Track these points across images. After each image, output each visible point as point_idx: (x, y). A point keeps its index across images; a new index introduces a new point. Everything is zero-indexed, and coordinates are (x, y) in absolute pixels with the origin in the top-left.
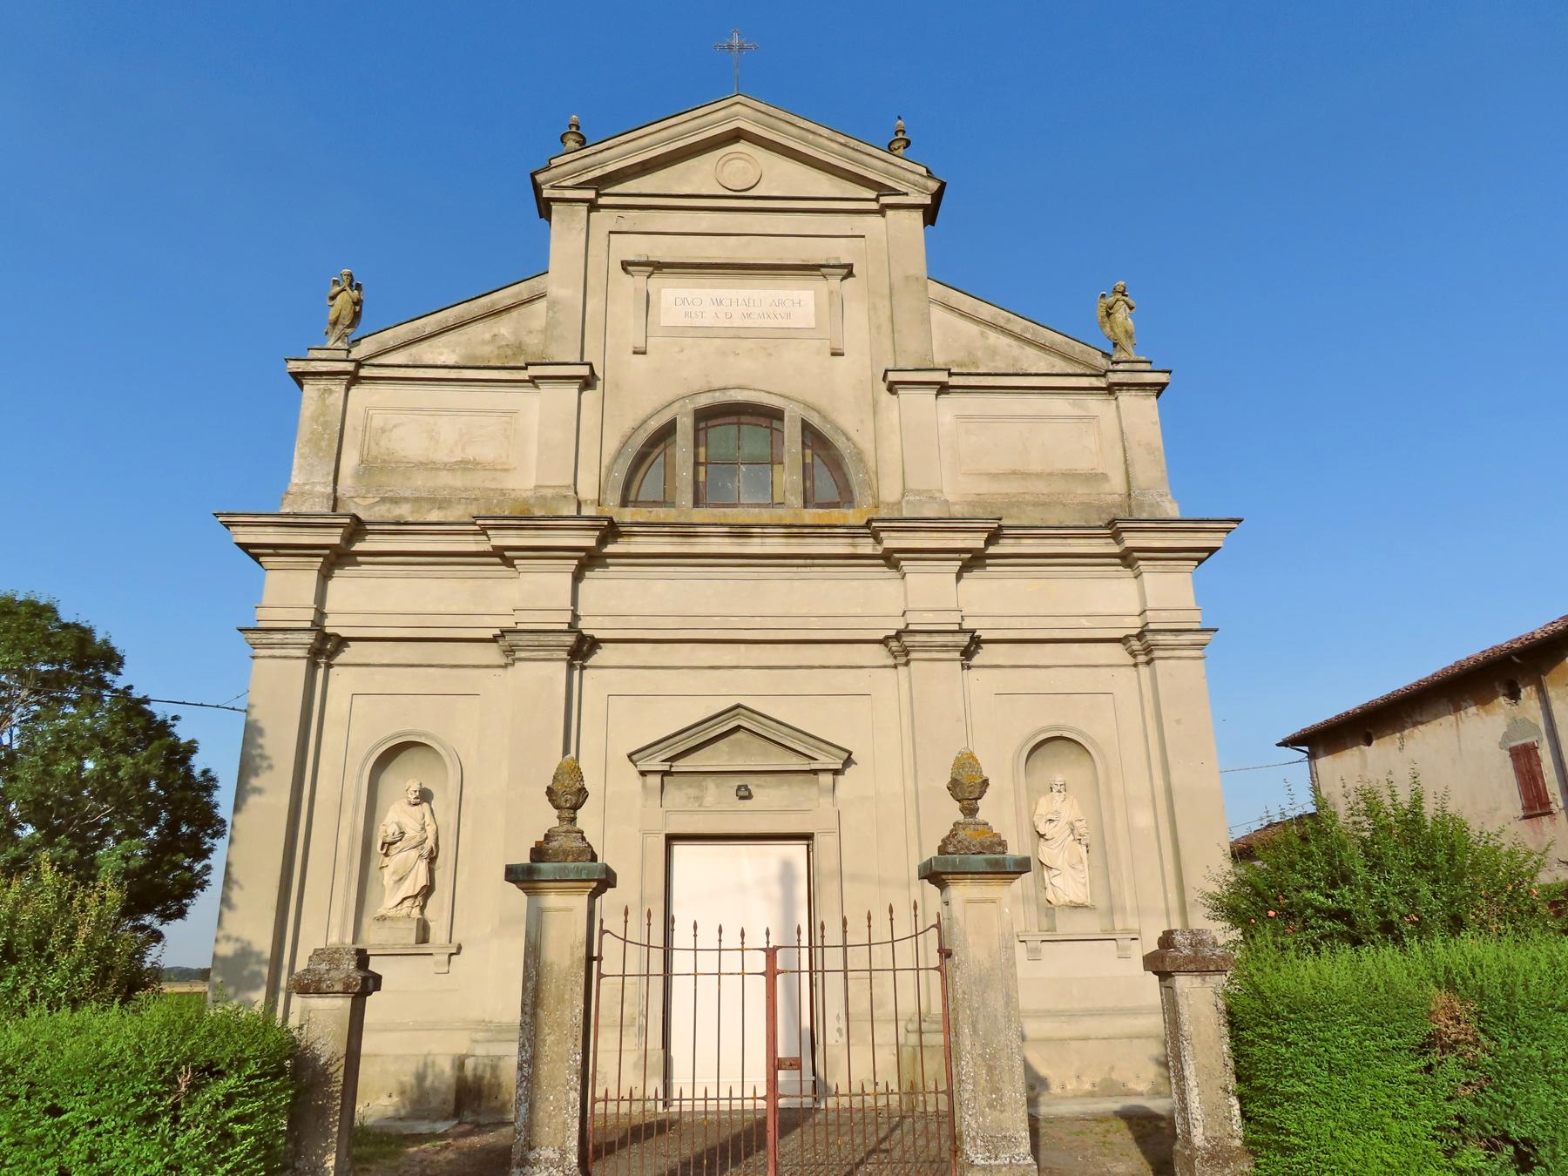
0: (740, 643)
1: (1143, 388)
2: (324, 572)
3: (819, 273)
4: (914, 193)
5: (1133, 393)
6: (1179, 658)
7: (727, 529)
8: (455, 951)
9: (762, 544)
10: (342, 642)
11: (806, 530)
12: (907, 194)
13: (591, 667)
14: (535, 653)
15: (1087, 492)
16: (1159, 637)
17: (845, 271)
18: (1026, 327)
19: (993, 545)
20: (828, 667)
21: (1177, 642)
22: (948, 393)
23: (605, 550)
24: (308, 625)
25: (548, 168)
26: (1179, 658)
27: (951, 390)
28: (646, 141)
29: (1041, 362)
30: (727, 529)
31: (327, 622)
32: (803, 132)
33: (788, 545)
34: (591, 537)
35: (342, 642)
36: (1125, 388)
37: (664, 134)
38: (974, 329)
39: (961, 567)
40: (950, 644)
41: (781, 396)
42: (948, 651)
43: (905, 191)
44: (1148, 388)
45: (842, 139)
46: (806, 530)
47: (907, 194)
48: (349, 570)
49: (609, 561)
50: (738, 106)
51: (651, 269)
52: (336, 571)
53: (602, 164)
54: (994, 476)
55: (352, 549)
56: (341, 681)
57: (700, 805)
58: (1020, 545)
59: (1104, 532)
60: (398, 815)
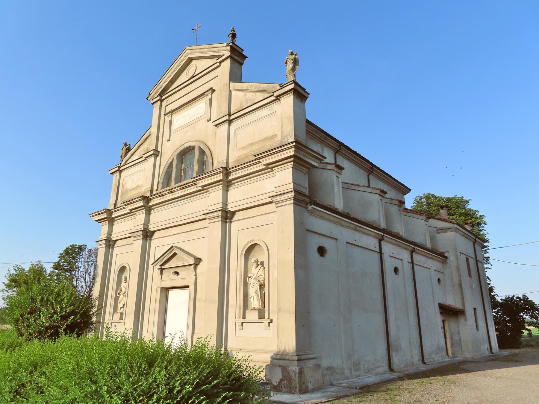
0: (185, 224)
1: (287, 93)
2: (226, 189)
3: (205, 95)
4: (226, 53)
5: (285, 97)
6: (284, 205)
7: (168, 191)
8: (270, 324)
9: (235, 174)
10: (234, 213)
11: (184, 186)
12: (224, 55)
13: (115, 247)
14: (138, 238)
15: (270, 144)
16: (276, 198)
17: (210, 91)
18: (251, 86)
19: (230, 176)
20: (203, 228)
21: (282, 199)
22: (233, 122)
23: (149, 205)
24: (292, 190)
25: (149, 95)
26: (284, 205)
27: (233, 121)
28: (168, 75)
29: (260, 96)
30: (168, 191)
31: (228, 207)
32: (200, 50)
33: (183, 192)
34: (142, 202)
35: (234, 213)
36: (281, 96)
37: (172, 70)
38: (242, 94)
39: (145, 211)
40: (217, 216)
41: (180, 147)
42: (218, 218)
43: (223, 54)
44: (289, 93)
45: (207, 46)
46: (184, 186)
47: (224, 55)
48: (232, 187)
49: (233, 182)
50: (187, 51)
51: (170, 114)
52: (229, 188)
53: (161, 87)
54: (244, 148)
55: (229, 179)
56: (235, 226)
57: (169, 278)
58: (237, 174)
59: (113, 211)
60: (254, 271)
